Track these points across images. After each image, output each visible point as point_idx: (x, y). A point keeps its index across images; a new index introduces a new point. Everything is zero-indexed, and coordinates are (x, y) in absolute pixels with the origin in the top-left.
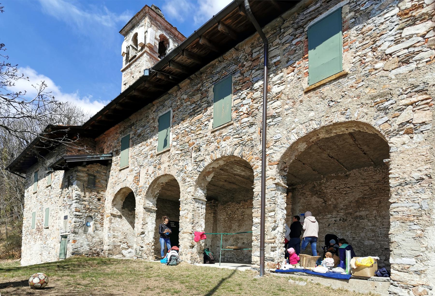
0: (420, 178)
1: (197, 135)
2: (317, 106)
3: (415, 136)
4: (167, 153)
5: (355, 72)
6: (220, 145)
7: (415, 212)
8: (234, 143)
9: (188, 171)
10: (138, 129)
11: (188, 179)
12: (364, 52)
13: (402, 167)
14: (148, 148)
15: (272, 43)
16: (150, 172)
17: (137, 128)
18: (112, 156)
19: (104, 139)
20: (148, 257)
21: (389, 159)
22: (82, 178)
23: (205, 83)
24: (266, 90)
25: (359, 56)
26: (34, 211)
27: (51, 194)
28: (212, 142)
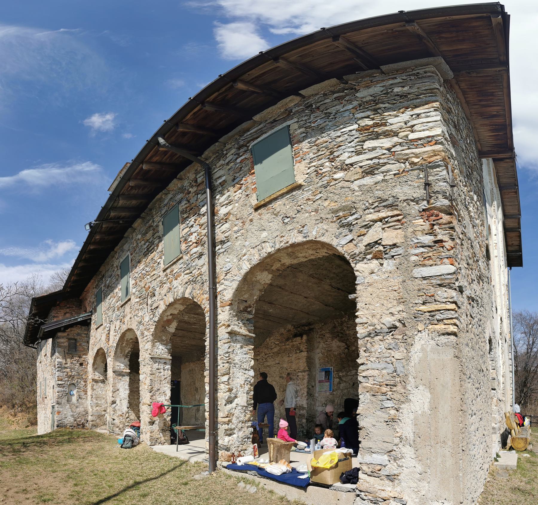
0: (393, 325)
2: (270, 224)
3: (385, 262)
5: (310, 182)
7: (388, 378)
8: (185, 281)
12: (320, 162)
13: (371, 307)
20: (121, 432)
21: (355, 295)
22: (63, 345)
25: (314, 166)
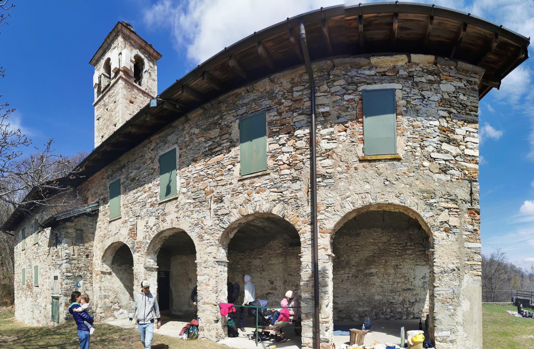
1: (217, 181)
3: (450, 235)
4: (174, 201)
6: (252, 198)
8: (271, 198)
9: (207, 227)
10: (131, 173)
11: (206, 236)
14: (146, 195)
15: (319, 87)
16: (151, 224)
17: (130, 171)
18: (99, 206)
19: (88, 187)
23: (225, 115)
24: (312, 142)
26: (23, 267)
27: (38, 251)
28: (239, 193)
